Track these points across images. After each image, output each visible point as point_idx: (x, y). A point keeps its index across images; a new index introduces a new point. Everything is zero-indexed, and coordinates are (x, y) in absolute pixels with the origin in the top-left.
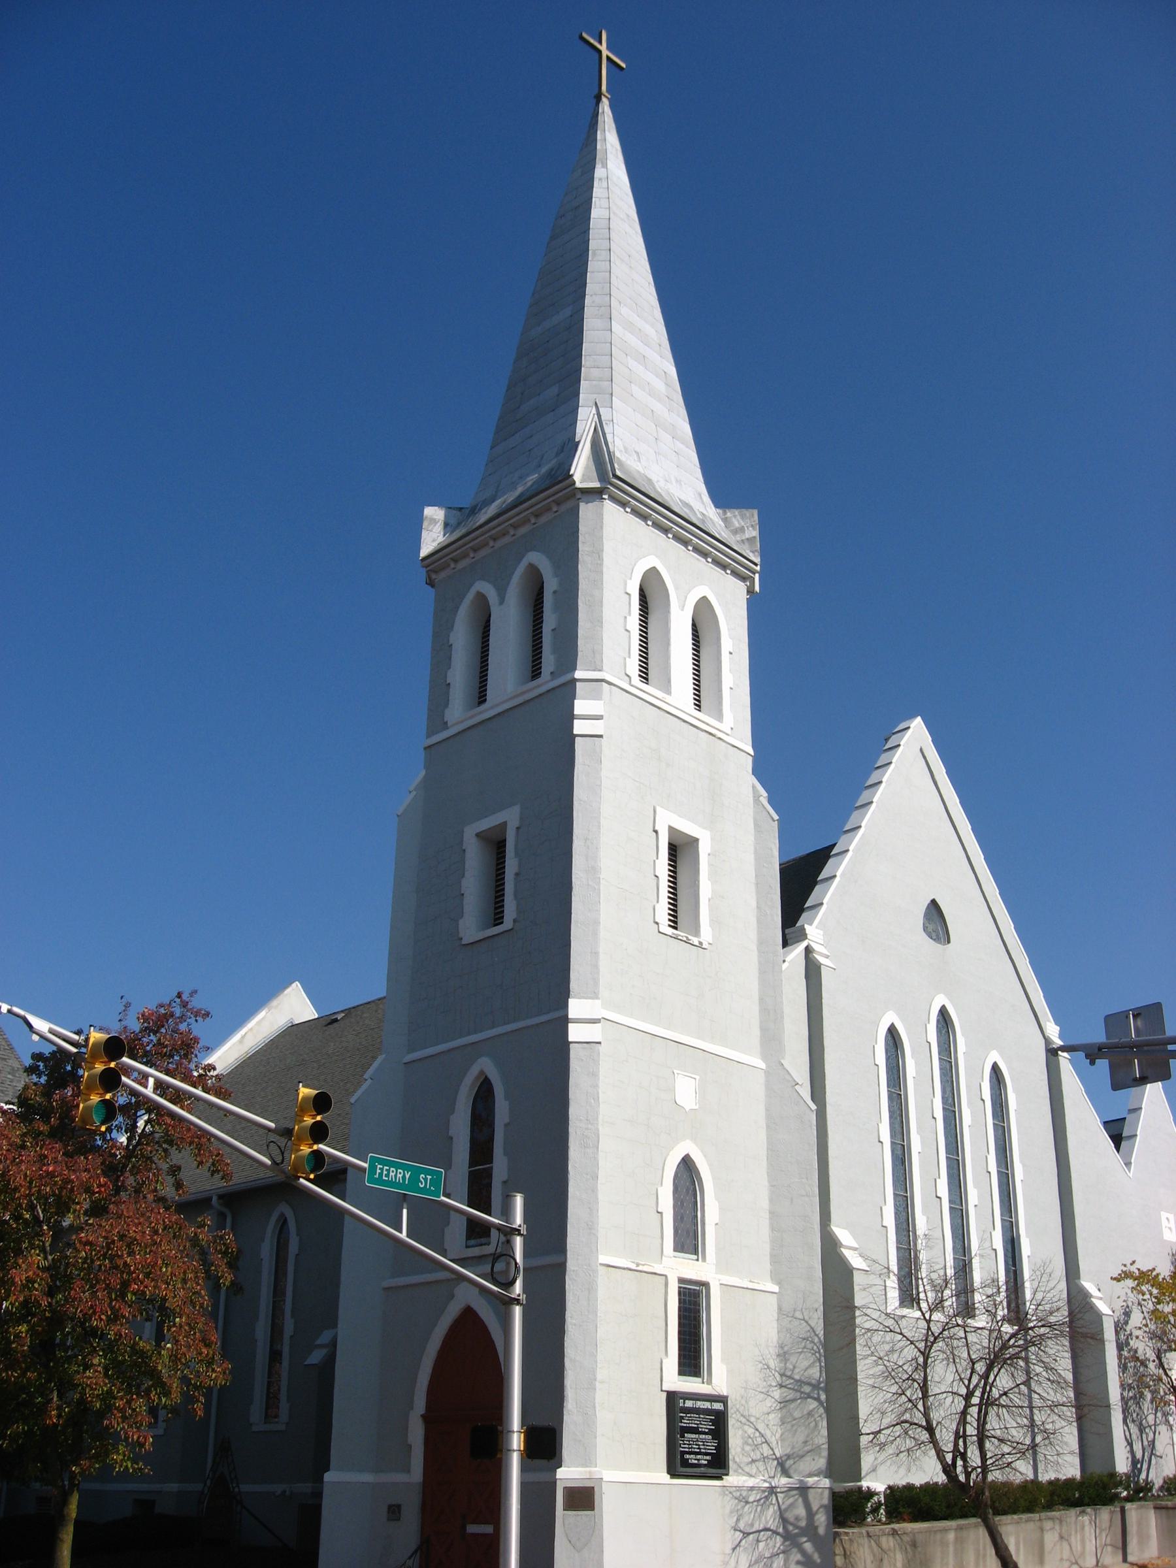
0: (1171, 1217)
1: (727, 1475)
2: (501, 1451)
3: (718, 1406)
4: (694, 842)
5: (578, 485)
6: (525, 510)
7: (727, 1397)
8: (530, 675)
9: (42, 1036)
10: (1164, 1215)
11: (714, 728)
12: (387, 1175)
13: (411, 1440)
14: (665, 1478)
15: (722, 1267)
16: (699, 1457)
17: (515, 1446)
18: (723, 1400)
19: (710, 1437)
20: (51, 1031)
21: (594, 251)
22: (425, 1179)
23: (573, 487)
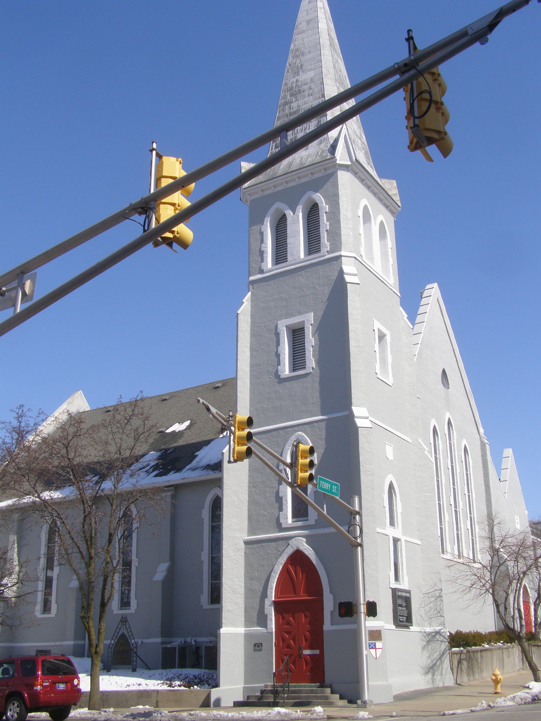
0: (518, 518)
1: (412, 626)
2: (356, 613)
3: (408, 595)
4: (385, 335)
5: (338, 162)
6: (294, 175)
7: (410, 591)
8: (308, 253)
9: (214, 416)
10: (516, 517)
11: (387, 282)
12: (324, 486)
13: (56, 605)
14: (394, 627)
15: (404, 533)
16: (403, 617)
17: (362, 611)
18: (409, 592)
19: (405, 609)
20: (217, 413)
21: (323, 45)
22: (334, 488)
23: (334, 163)
